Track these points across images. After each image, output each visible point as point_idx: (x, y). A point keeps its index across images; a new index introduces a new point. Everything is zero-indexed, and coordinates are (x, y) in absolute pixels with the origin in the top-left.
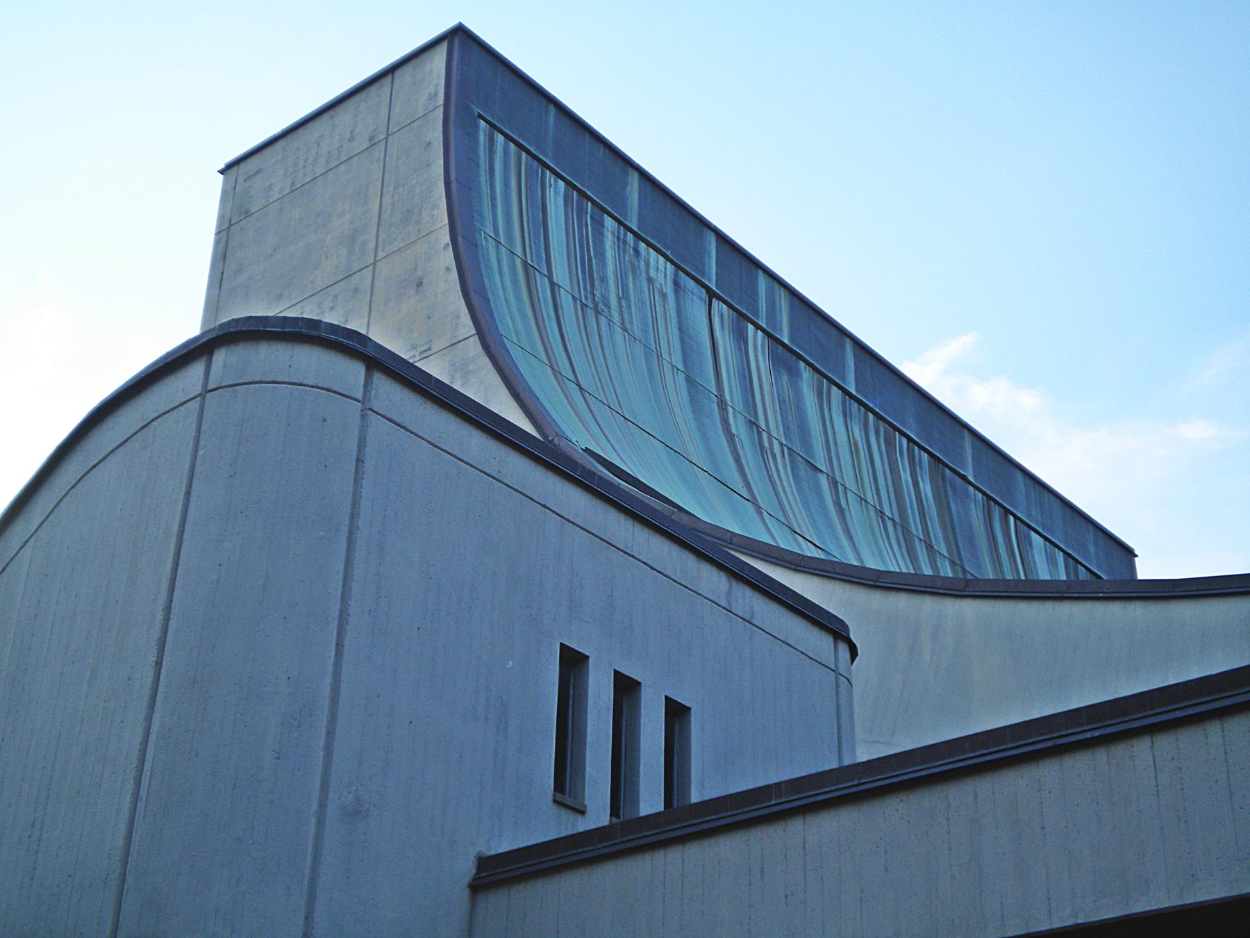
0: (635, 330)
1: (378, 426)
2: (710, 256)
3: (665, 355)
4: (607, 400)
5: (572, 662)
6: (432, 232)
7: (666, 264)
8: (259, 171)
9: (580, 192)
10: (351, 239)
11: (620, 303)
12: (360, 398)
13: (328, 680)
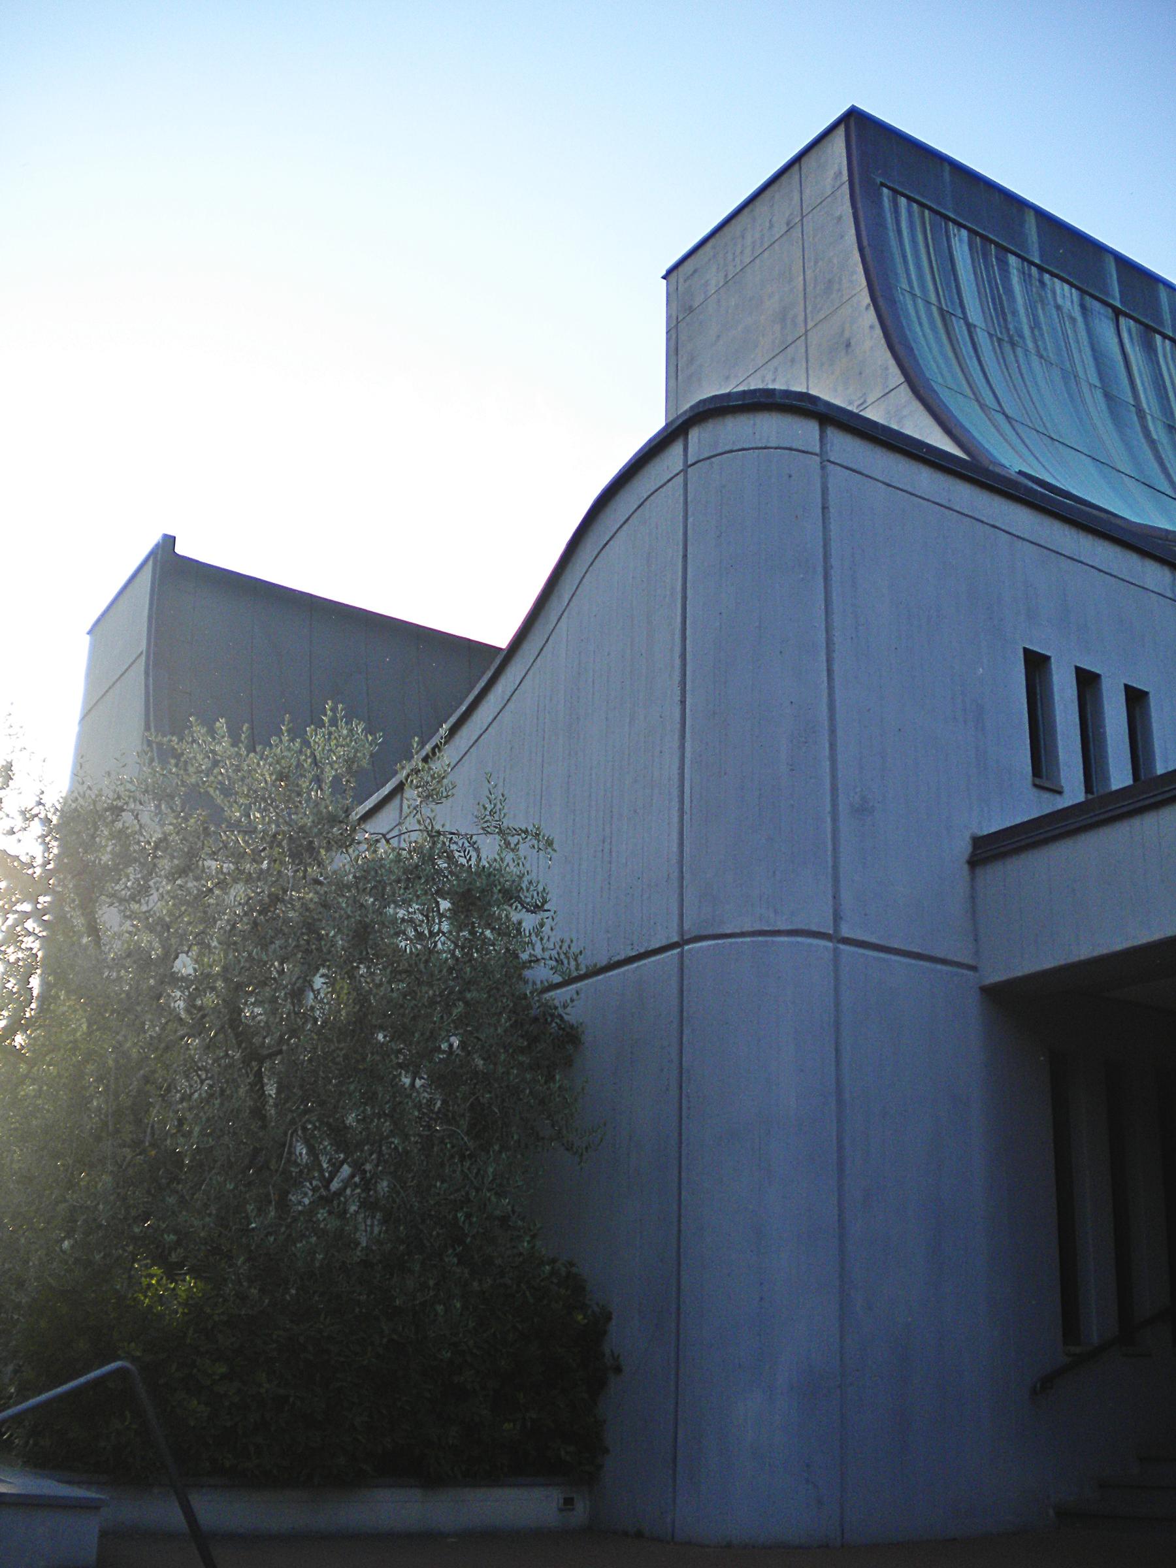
0: (1051, 355)
1: (838, 477)
2: (1111, 276)
3: (1081, 374)
4: (1032, 422)
5: (1036, 664)
6: (853, 296)
7: (1071, 290)
8: (695, 271)
9: (982, 237)
10: (783, 316)
11: (1032, 332)
12: (817, 450)
13: (825, 699)
